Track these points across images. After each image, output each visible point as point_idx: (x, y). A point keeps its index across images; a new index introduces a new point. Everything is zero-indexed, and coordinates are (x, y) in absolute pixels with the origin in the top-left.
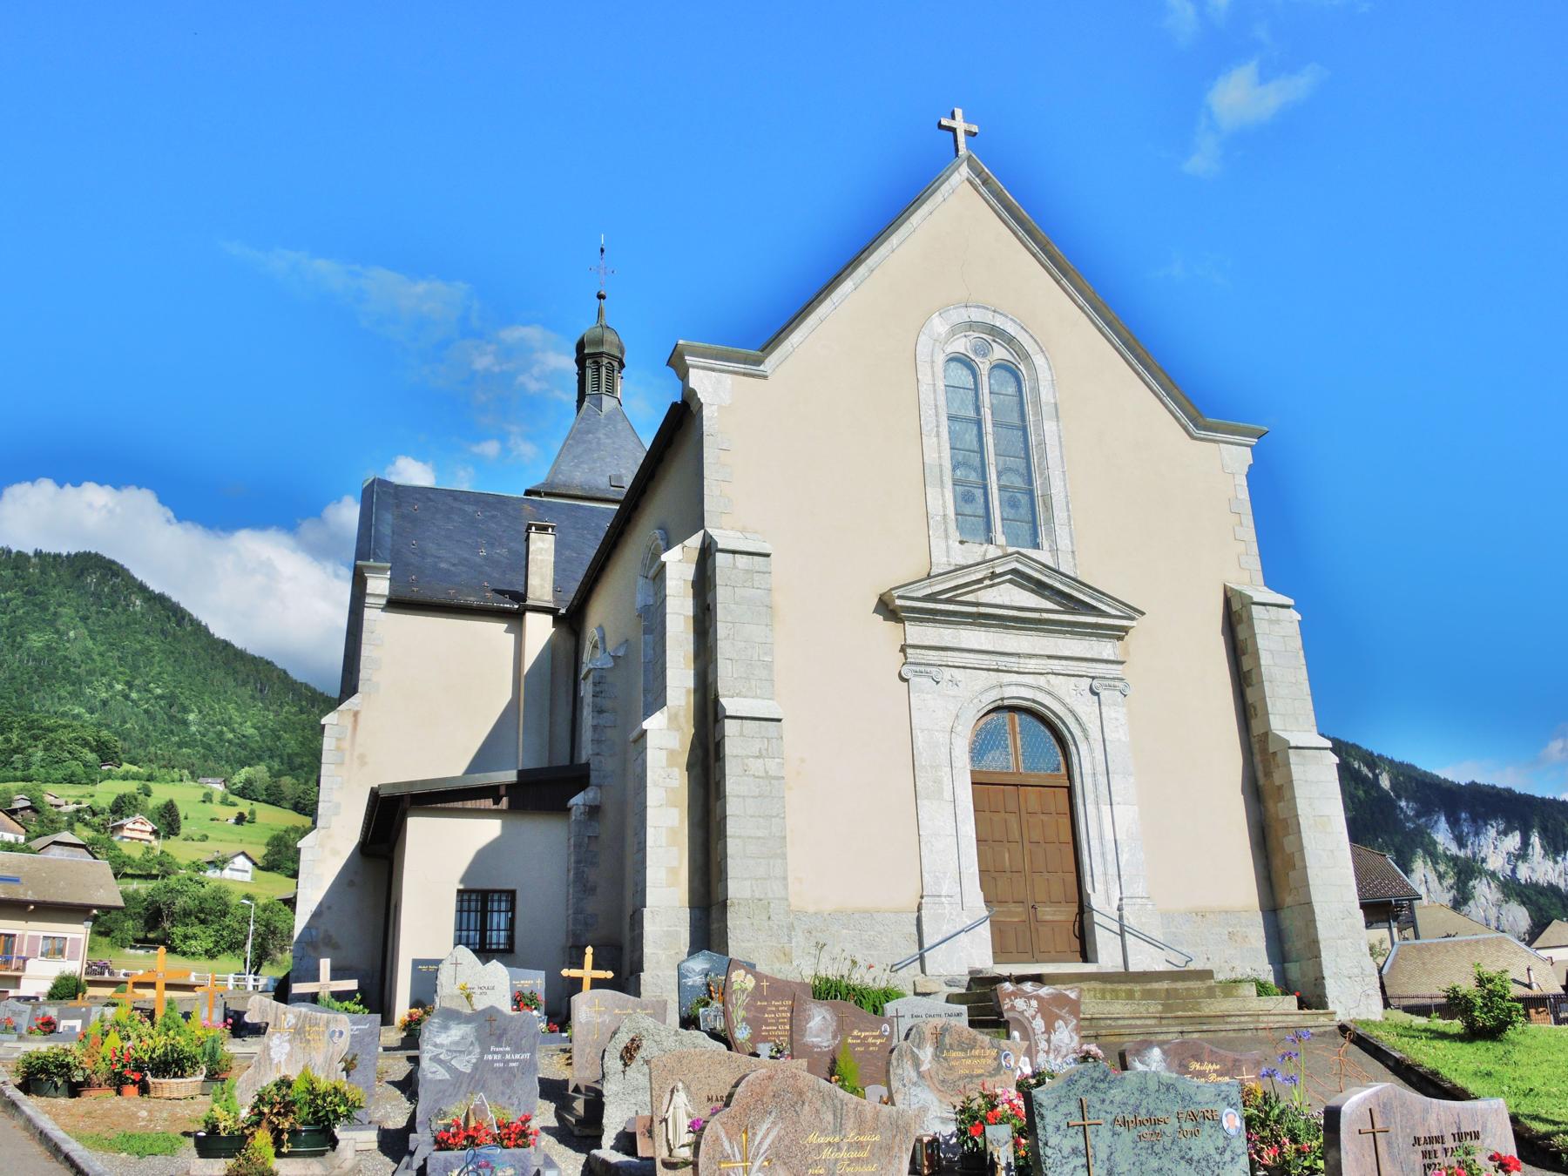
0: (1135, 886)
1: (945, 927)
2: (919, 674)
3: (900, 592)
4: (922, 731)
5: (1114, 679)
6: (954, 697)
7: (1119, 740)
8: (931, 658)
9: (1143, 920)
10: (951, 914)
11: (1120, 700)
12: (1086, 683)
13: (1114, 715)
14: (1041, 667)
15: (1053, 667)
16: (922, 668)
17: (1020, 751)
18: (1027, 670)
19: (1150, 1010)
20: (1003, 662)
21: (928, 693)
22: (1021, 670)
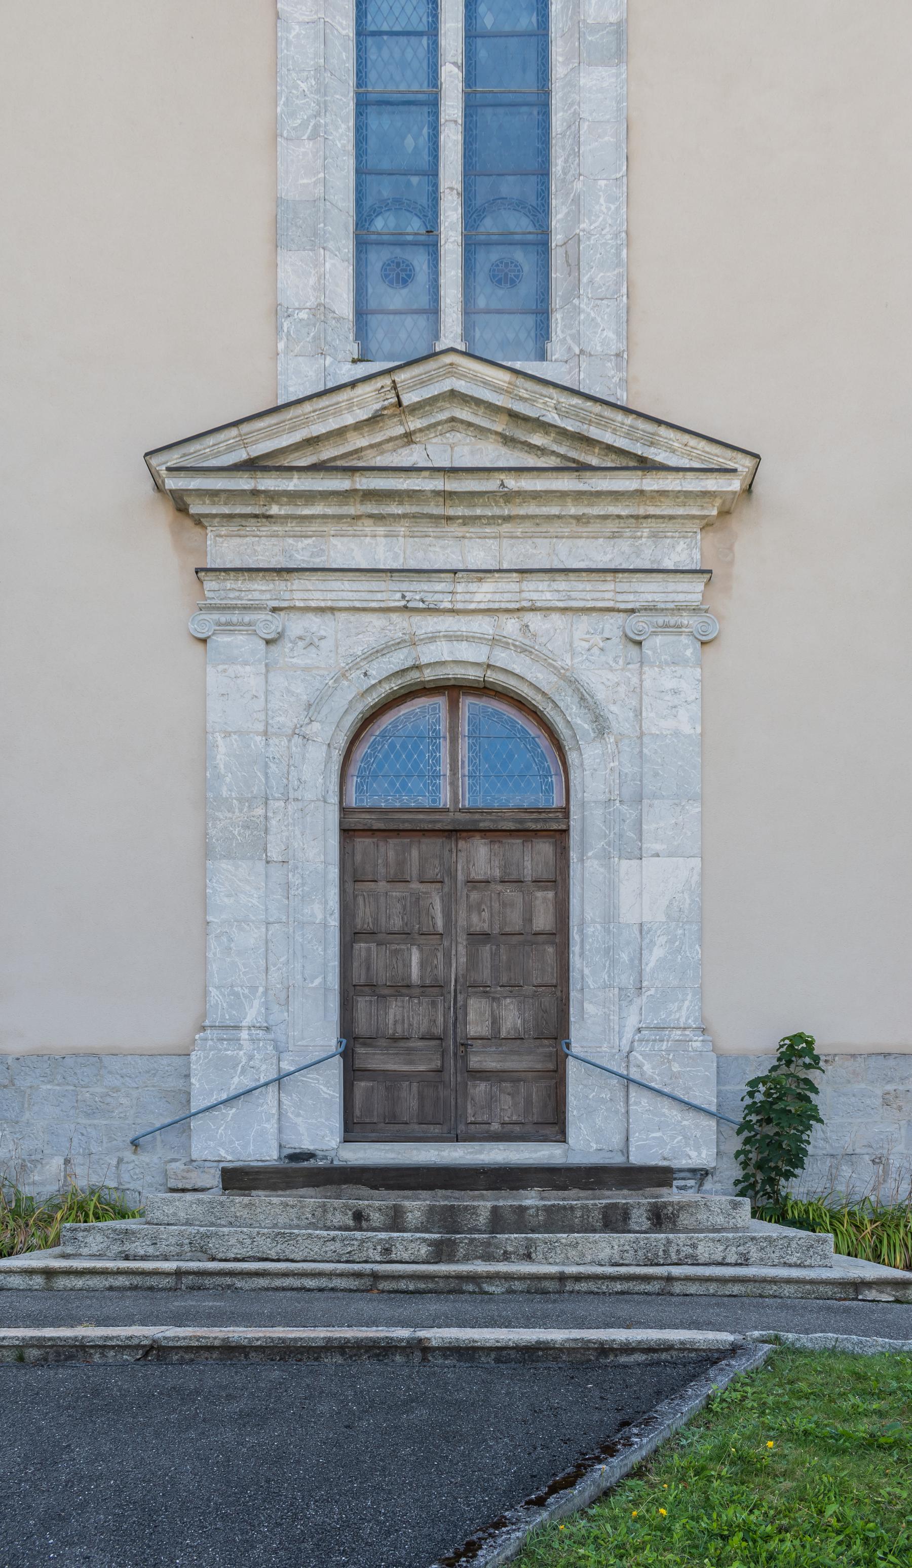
0: (674, 1007)
1: (236, 1080)
2: (228, 628)
3: (174, 458)
4: (227, 734)
5: (679, 609)
6: (306, 669)
7: (676, 733)
8: (257, 595)
9: (676, 1068)
10: (251, 1058)
11: (689, 653)
12: (612, 624)
13: (669, 683)
14: (507, 596)
15: (535, 596)
16: (235, 617)
17: (465, 769)
18: (473, 606)
19: (399, 1252)
20: (417, 591)
21: (246, 663)
22: (459, 606)
